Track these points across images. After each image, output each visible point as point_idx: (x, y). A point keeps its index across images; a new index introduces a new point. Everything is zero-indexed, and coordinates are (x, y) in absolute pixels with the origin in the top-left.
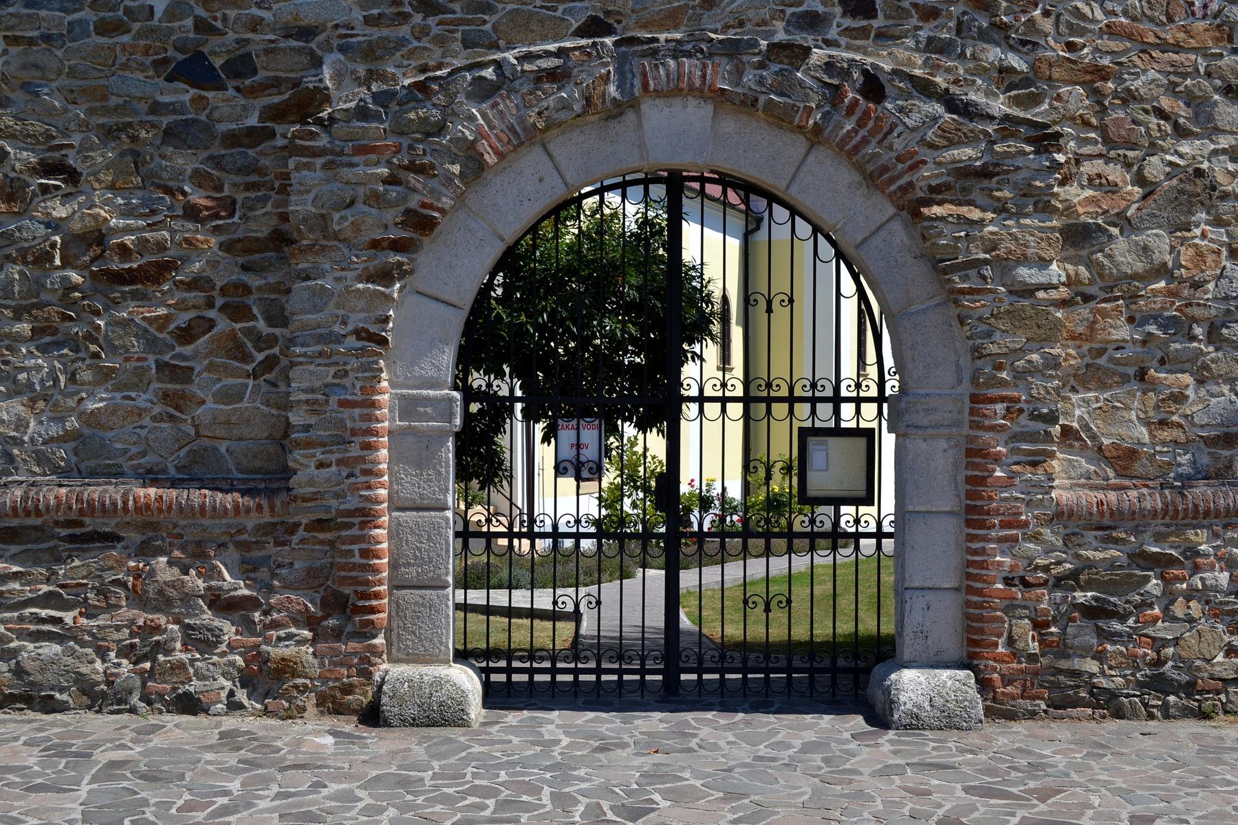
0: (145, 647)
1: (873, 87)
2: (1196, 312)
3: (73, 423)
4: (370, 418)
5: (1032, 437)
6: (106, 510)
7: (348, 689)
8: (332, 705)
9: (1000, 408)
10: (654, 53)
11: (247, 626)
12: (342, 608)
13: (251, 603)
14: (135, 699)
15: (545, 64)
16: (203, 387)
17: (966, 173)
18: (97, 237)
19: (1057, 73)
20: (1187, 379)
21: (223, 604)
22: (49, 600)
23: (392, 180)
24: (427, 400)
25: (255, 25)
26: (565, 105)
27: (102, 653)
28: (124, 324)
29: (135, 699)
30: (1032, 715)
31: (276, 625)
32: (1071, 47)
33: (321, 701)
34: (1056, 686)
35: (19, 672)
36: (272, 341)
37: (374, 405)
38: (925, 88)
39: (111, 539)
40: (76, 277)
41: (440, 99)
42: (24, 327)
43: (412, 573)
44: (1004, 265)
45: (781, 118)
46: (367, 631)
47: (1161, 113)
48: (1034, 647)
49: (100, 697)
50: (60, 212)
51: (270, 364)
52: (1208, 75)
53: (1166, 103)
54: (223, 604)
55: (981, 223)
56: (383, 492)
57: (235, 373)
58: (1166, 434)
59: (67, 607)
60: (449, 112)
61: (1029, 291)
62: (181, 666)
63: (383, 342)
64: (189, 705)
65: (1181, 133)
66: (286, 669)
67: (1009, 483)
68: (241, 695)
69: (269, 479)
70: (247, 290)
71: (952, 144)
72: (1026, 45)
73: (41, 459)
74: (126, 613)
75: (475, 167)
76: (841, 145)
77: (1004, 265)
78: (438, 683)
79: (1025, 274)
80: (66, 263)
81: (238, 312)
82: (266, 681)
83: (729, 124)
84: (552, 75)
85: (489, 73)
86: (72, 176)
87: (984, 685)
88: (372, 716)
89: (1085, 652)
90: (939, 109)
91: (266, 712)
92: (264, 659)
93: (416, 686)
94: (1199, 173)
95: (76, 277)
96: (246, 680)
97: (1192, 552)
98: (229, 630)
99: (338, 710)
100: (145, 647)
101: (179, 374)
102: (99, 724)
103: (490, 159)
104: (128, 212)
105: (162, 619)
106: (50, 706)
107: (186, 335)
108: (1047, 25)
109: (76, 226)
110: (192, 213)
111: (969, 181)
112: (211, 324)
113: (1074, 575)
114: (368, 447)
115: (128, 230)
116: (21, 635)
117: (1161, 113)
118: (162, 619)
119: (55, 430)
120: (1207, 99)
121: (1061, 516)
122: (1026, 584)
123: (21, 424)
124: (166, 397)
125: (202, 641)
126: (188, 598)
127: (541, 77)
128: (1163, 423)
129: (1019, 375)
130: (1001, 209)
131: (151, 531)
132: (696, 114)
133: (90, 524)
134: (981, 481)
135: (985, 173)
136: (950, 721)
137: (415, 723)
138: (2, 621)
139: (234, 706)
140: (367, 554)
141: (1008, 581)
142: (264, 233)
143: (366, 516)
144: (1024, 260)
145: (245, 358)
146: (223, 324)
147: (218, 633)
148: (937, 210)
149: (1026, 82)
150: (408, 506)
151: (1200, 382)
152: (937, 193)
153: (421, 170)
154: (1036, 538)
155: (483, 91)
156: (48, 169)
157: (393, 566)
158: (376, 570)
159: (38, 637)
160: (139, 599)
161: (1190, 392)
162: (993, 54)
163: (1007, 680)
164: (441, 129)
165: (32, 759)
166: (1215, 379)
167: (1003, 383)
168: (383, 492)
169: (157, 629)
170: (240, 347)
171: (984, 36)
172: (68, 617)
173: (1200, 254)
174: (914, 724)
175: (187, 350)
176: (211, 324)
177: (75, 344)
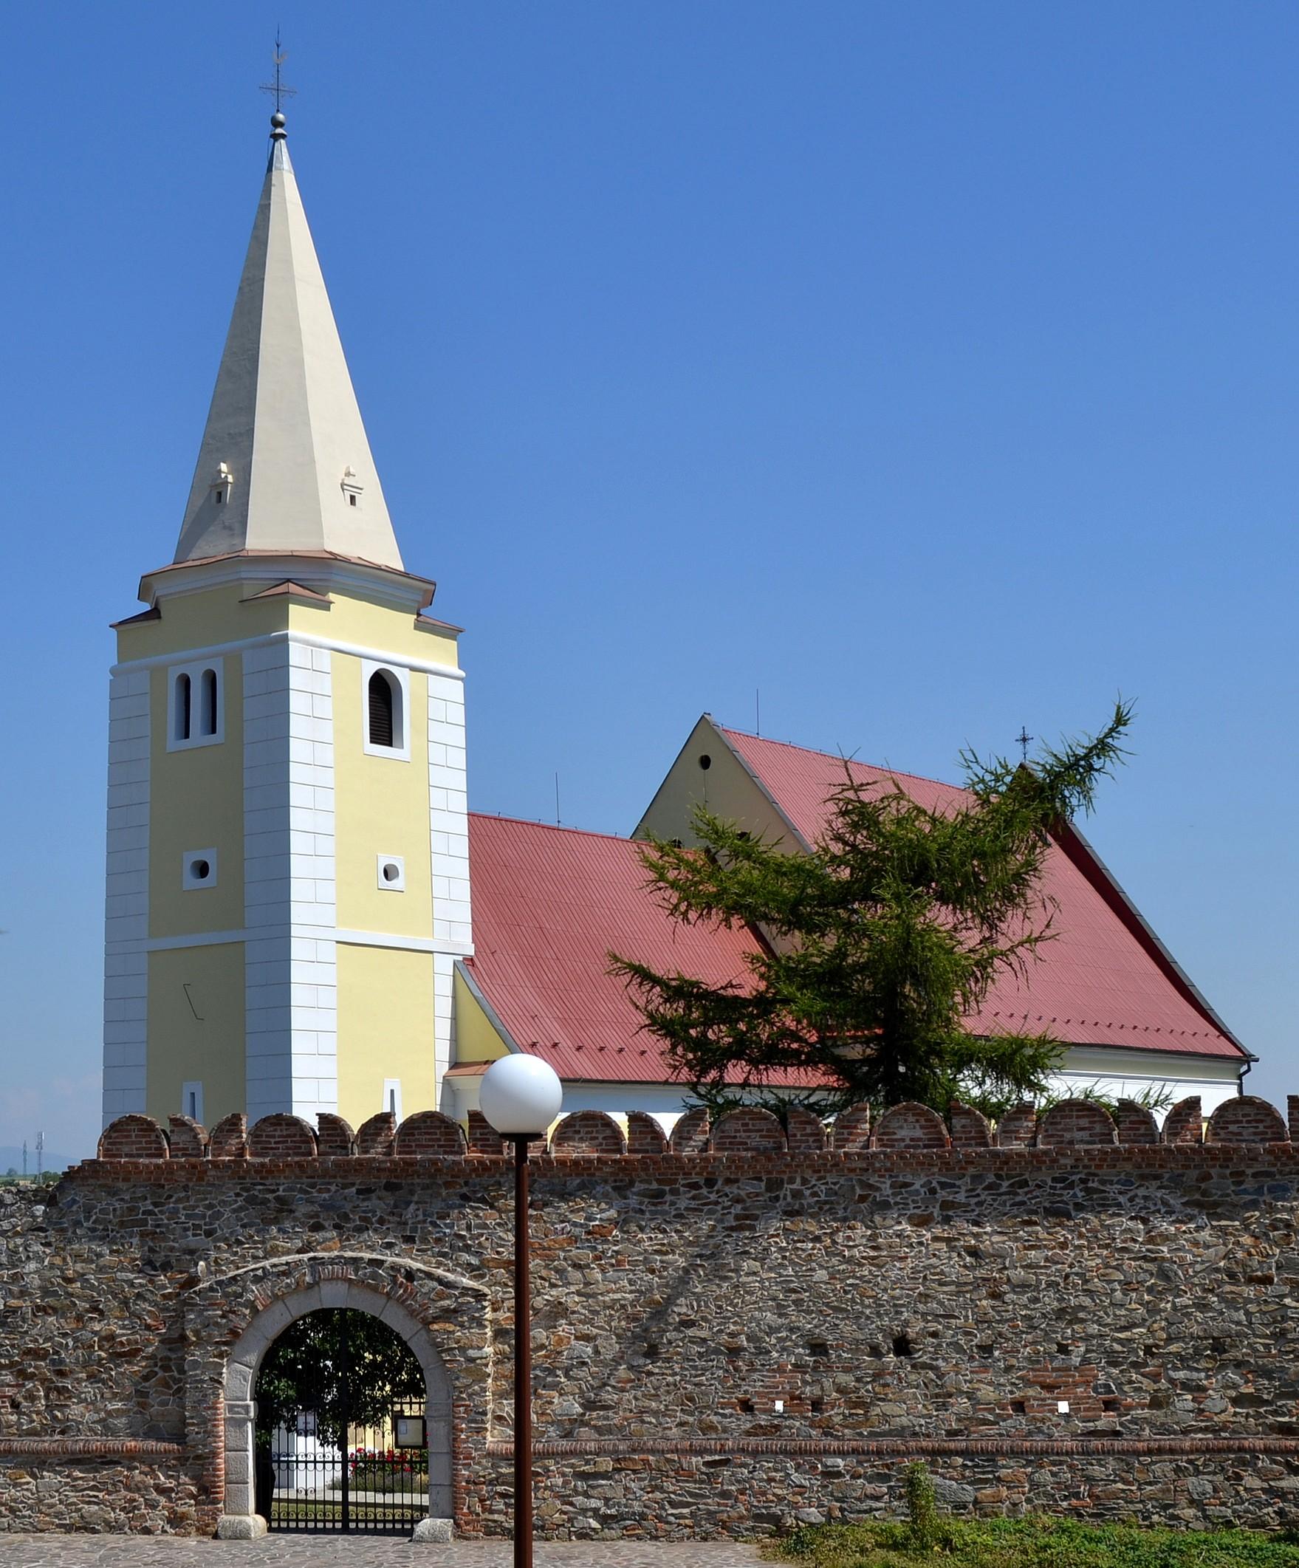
0: (130, 1507)
1: (410, 1275)
2: (557, 1365)
3: (103, 1415)
4: (215, 1414)
5: (475, 1421)
6: (116, 1452)
7: (208, 1525)
8: (202, 1531)
9: (462, 1409)
10: (323, 1264)
11: (170, 1499)
12: (206, 1491)
13: (171, 1490)
14: (126, 1529)
15: (281, 1268)
16: (154, 1400)
17: (446, 1310)
18: (111, 1337)
19: (491, 1264)
20: (555, 1394)
21: (161, 1490)
22: (93, 1488)
23: (223, 1316)
24: (238, 1406)
25: (172, 1249)
26: (288, 1285)
27: (114, 1509)
28: (122, 1374)
29: (126, 1529)
30: (477, 1538)
31: (180, 1499)
32: (498, 1253)
33: (198, 1529)
34: (487, 1526)
35: (82, 1517)
36: (180, 1380)
37: (217, 1409)
38: (429, 1275)
39: (118, 1463)
40: (103, 1354)
41: (240, 1283)
42: (84, 1375)
43: (233, 1477)
44: (463, 1350)
45: (375, 1289)
46: (216, 1501)
47: (542, 1278)
48: (479, 1510)
49: (112, 1527)
50: (97, 1327)
51: (179, 1390)
52: (565, 1259)
53: (544, 1273)
54: (161, 1490)
55: (453, 1332)
56: (221, 1444)
57: (165, 1394)
58: (543, 1419)
59: (100, 1491)
60: (245, 1289)
61: (473, 1360)
62: (143, 1515)
63: (220, 1383)
64: (147, 1531)
65: (553, 1286)
66: (184, 1517)
67: (466, 1441)
68: (167, 1528)
69: (180, 1438)
70: (170, 1359)
71: (442, 1299)
72: (478, 1254)
73: (91, 1430)
74: (123, 1492)
75: (255, 1311)
76: (398, 1300)
77: (463, 1350)
78: (240, 1522)
79: (471, 1353)
80: (100, 1348)
81: (166, 1368)
82: (176, 1521)
83: (355, 1291)
84: (284, 1273)
85: (260, 1272)
86: (101, 1313)
87: (457, 1525)
88: (216, 1536)
89: (499, 1512)
90: (435, 1284)
91: (176, 1534)
92: (175, 1512)
93: (232, 1524)
94: (560, 1303)
95: (103, 1354)
96: (170, 1521)
97: (547, 1470)
98: (163, 1500)
99: (205, 1533)
100: (130, 1507)
101: (144, 1394)
102: (112, 1538)
103: (260, 1308)
104: (124, 1327)
105: (137, 1496)
106: (94, 1531)
107: (146, 1378)
108: (487, 1244)
109: (103, 1334)
110: (148, 1327)
111: (448, 1315)
112: (156, 1373)
113: (497, 1479)
114: (215, 1426)
115: (123, 1335)
116: (83, 1502)
117: (542, 1278)
118: (137, 1496)
119: (96, 1417)
120: (565, 1270)
121: (490, 1454)
122: (475, 1483)
123: (83, 1416)
124: (139, 1404)
125: (152, 1505)
126: (146, 1488)
127: (279, 1274)
128: (543, 1414)
129: (470, 1396)
130: (462, 1326)
131: (130, 1458)
132: (342, 1287)
133: (109, 1457)
134: (454, 1440)
135: (455, 1311)
136: (436, 1539)
137: (230, 1538)
138: (3, 1233)
139: (164, 1532)
140: (215, 1470)
141: (468, 1482)
142: (176, 1336)
143: (215, 1455)
144: (472, 1347)
145: (170, 1388)
146: (161, 1374)
147: (158, 1502)
148: (435, 1327)
149: (478, 1268)
150: (236, 1450)
151: (561, 1395)
152: (436, 1319)
153: (234, 1312)
154: (479, 1463)
155: (257, 1280)
156: (95, 1309)
157: (226, 1474)
158: (218, 1476)
159: (89, 1503)
160: (128, 1488)
161: (556, 1401)
162: (465, 1257)
163: (467, 1523)
164: (241, 1296)
165: (86, 1546)
166: (566, 1394)
167: (464, 1399)
168: (221, 1444)
169: (135, 1500)
170: (167, 1383)
171: (460, 1250)
172: (101, 1495)
173: (561, 1339)
174: (421, 1540)
175: (147, 1384)
176: (156, 1373)
177: (104, 1382)
